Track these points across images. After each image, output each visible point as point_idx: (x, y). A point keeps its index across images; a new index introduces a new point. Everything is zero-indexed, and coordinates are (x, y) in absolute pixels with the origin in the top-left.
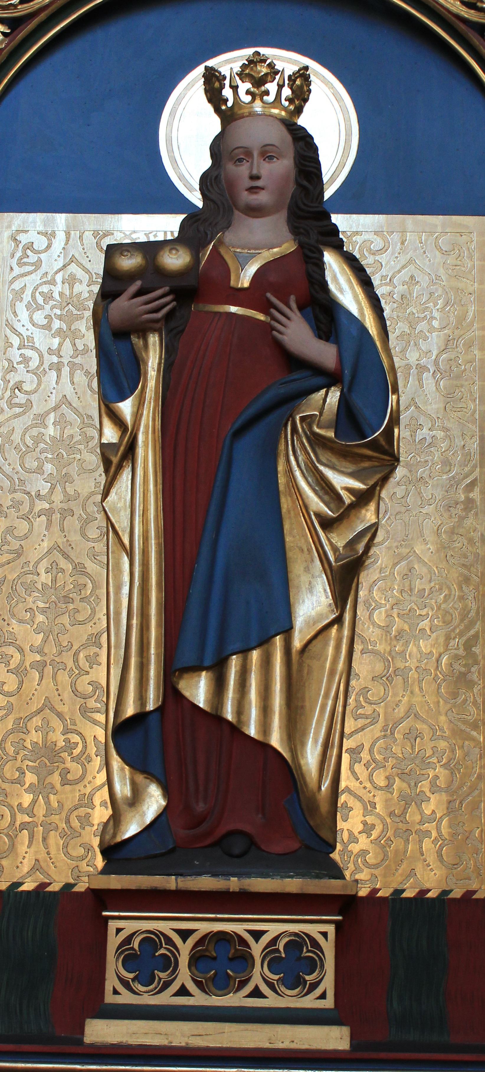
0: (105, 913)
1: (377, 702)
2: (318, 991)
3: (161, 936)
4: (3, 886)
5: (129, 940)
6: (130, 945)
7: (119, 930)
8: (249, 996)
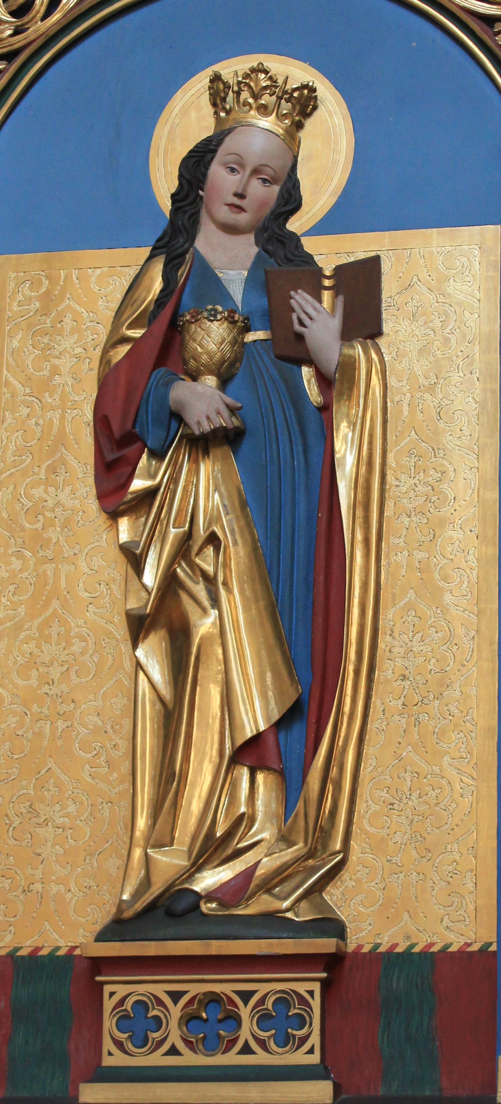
0: (98, 978)
1: (425, 803)
2: (307, 1047)
3: (294, 996)
4: (3, 952)
5: (122, 1002)
6: (264, 1005)
7: (112, 994)
8: (167, 1054)
